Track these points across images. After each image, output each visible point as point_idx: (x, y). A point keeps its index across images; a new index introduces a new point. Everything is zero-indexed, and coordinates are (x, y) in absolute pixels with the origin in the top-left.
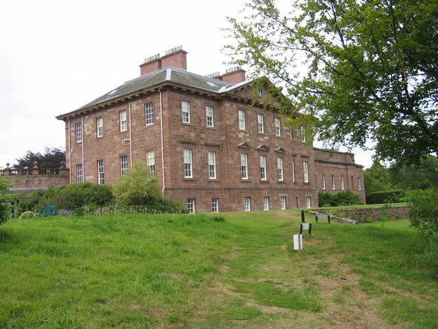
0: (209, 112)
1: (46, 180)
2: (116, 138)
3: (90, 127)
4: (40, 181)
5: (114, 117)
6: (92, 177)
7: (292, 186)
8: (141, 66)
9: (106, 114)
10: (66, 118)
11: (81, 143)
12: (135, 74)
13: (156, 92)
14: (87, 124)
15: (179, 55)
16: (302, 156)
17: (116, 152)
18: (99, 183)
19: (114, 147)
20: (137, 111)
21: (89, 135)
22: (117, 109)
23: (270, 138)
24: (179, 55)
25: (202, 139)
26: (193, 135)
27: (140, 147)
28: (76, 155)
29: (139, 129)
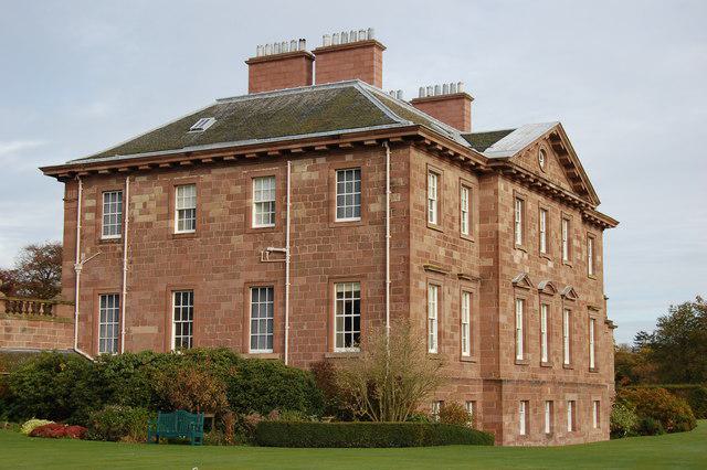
0: (343, 192)
1: (24, 330)
2: (237, 240)
3: (152, 205)
4: (8, 330)
5: (237, 189)
6: (153, 330)
7: (581, 378)
8: (251, 63)
9: (205, 177)
10: (67, 175)
11: (120, 241)
12: (235, 85)
13: (379, 146)
14: (140, 198)
15: (362, 52)
16: (589, 307)
17: (235, 276)
18: (173, 347)
19: (232, 262)
20: (311, 183)
21: (149, 225)
22: (243, 172)
23: (555, 266)
24: (362, 52)
25: (454, 262)
26: (442, 251)
27: (318, 272)
28: (101, 272)
29: (317, 226)
